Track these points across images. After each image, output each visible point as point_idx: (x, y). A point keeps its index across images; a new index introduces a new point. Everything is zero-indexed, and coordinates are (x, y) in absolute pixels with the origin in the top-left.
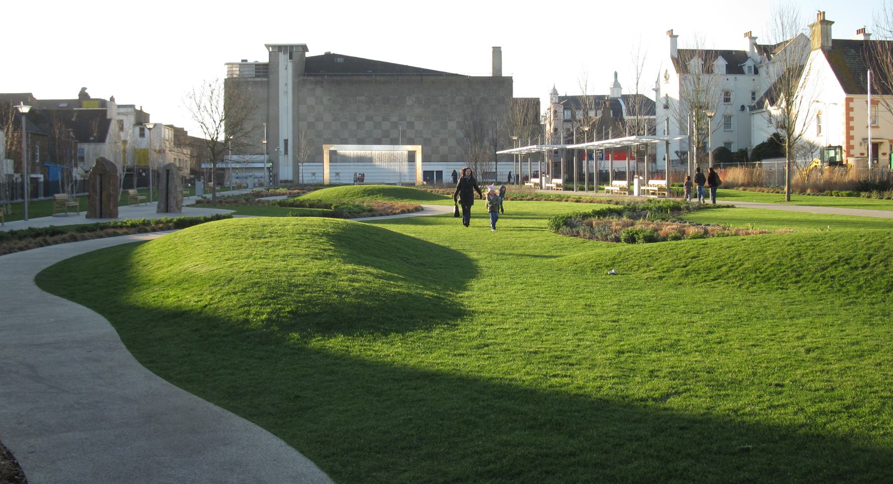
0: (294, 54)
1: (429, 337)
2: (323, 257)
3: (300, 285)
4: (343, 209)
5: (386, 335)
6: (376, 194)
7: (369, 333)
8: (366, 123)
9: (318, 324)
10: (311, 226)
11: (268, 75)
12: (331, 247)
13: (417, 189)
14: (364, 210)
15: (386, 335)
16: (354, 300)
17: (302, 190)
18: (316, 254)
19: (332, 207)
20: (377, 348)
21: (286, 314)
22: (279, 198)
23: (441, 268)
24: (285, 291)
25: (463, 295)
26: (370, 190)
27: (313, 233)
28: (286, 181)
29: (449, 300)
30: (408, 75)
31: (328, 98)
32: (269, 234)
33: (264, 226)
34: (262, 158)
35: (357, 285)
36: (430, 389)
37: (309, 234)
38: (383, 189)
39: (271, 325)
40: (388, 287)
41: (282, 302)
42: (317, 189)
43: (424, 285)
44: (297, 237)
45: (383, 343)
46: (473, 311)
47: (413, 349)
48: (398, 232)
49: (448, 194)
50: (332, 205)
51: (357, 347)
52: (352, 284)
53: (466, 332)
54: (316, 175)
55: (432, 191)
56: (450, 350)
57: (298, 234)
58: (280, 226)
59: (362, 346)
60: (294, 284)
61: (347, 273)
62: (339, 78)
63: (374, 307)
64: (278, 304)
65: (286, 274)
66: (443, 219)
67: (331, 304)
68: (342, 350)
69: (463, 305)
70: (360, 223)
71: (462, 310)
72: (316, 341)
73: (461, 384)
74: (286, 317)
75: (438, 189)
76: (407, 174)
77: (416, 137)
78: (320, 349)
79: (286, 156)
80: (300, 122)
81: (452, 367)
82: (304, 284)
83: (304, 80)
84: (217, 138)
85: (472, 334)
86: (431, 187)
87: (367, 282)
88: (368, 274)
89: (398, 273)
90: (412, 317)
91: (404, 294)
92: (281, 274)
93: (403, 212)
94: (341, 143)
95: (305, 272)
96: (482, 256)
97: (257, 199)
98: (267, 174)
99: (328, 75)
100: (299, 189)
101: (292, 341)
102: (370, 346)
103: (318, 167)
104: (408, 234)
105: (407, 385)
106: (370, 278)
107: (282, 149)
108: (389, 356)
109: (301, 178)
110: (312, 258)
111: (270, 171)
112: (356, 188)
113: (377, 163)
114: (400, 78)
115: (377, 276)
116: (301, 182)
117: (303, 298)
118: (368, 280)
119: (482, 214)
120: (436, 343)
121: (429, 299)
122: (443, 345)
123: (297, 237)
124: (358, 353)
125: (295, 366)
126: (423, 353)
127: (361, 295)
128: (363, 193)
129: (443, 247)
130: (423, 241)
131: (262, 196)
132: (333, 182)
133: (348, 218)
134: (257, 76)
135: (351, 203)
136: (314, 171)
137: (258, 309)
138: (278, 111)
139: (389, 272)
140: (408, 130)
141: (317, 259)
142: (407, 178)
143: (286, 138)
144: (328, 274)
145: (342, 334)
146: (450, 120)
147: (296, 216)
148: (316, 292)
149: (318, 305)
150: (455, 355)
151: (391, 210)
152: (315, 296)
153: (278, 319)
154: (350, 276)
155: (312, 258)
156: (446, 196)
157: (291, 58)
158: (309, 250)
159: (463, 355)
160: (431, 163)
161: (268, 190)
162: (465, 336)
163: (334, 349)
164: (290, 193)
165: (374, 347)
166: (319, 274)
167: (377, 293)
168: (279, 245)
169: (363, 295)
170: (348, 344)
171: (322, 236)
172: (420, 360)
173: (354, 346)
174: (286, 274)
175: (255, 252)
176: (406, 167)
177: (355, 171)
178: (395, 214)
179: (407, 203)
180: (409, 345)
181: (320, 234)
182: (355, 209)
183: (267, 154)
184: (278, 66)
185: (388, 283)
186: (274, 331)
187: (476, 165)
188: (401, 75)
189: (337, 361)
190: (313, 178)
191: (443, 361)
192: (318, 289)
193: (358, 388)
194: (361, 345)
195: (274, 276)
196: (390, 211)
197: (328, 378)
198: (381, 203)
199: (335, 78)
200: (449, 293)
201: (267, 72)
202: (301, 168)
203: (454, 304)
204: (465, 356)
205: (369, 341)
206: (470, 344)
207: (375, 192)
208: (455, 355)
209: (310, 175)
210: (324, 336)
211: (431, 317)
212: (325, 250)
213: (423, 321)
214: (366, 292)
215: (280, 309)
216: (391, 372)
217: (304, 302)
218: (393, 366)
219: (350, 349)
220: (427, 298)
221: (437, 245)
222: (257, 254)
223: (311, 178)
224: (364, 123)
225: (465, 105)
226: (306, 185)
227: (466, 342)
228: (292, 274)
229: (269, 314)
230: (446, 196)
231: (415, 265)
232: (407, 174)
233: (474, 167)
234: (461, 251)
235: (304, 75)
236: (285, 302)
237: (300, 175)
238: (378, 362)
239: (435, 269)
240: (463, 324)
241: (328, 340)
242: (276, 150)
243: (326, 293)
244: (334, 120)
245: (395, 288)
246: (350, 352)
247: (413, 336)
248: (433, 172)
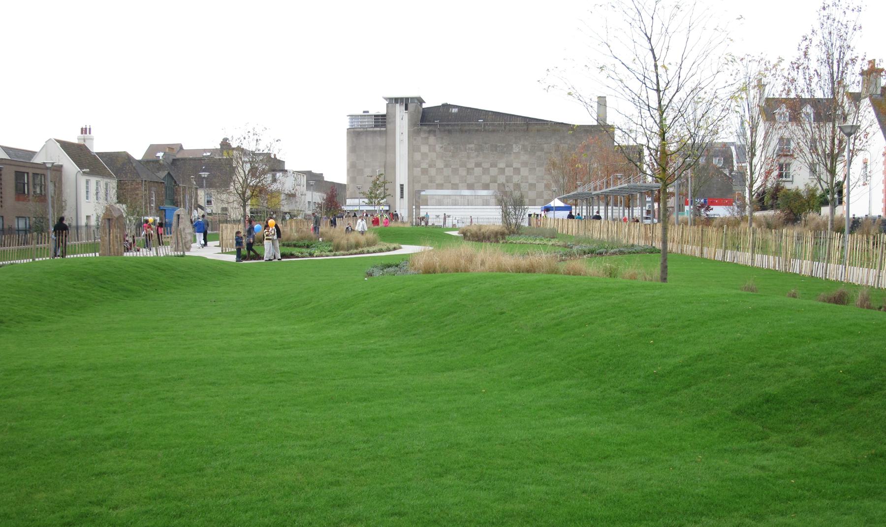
31: (441, 146)
134: (376, 126)
157: (406, 109)
184: (395, 117)
199: (447, 128)
224: (473, 169)
244: (446, 166)
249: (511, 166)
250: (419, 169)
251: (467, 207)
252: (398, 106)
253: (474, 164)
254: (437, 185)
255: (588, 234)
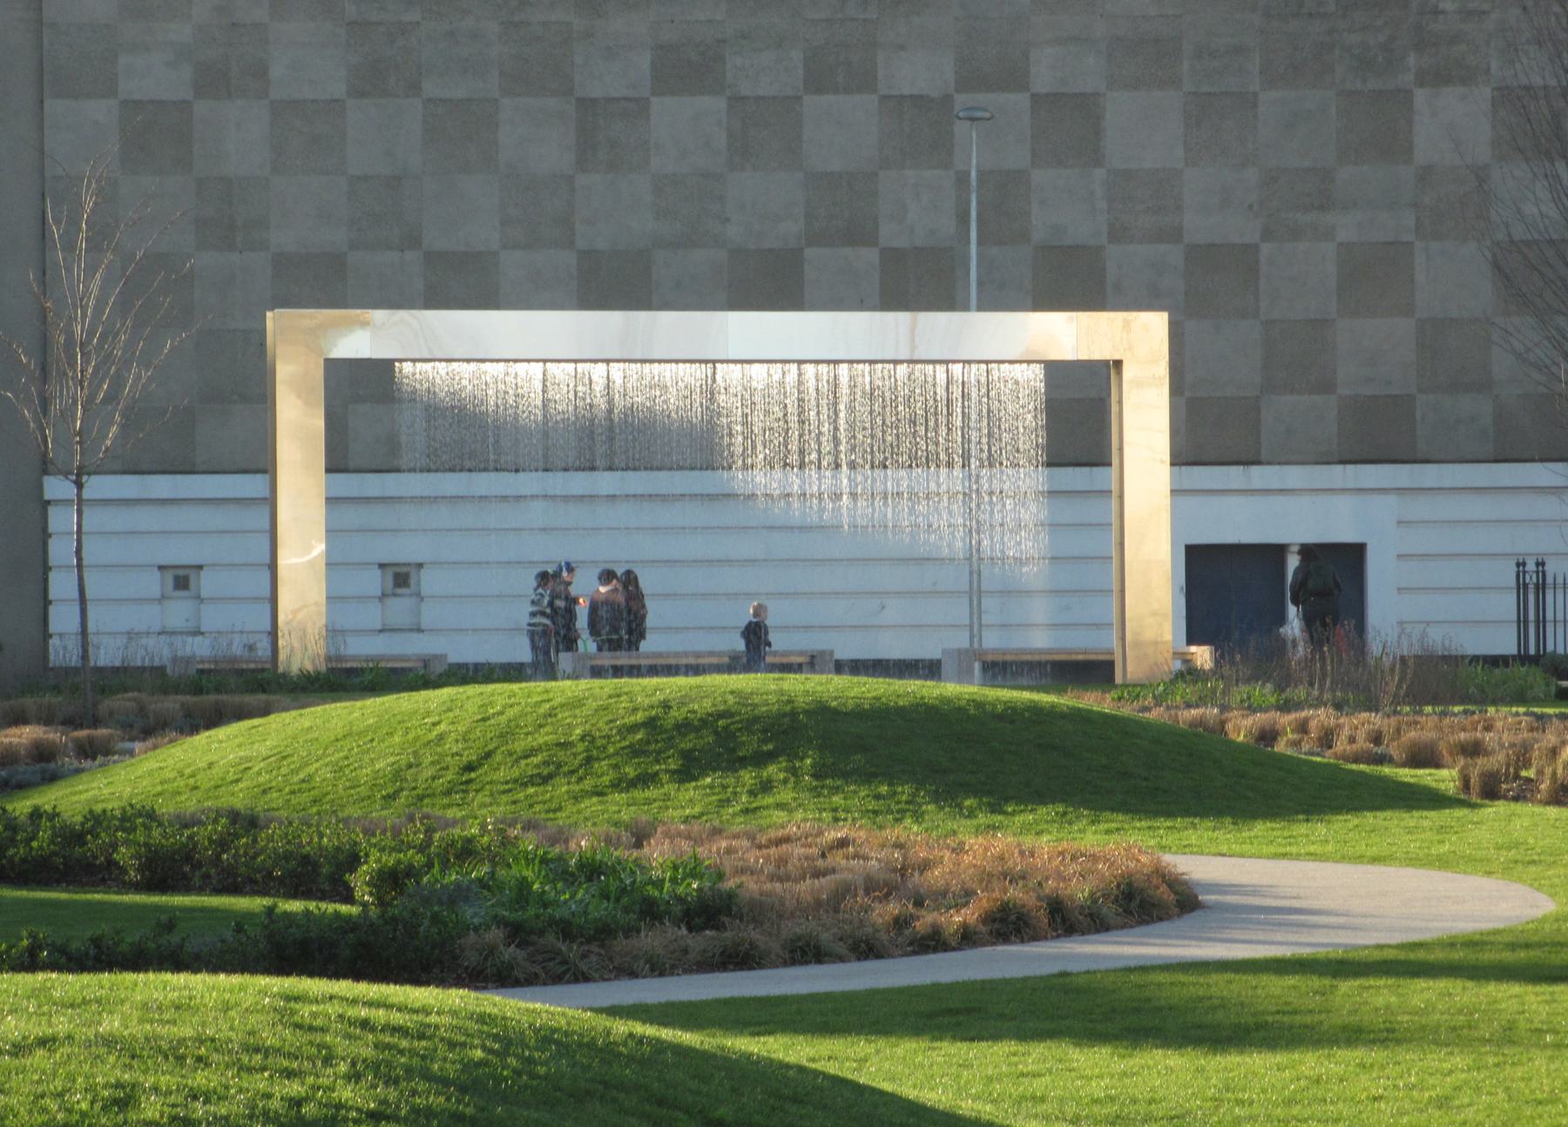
4: (459, 894)
6: (760, 760)
8: (808, 100)
10: (175, 1054)
13: (1126, 711)
14: (651, 912)
17: (71, 722)
19: (360, 881)
38: (823, 710)
42: (215, 718)
49: (1423, 757)
50: (353, 860)
54: (207, 583)
55: (1268, 736)
66: (1381, 995)
70: (621, 1028)
75: (1321, 717)
77: (1118, 234)
80: (54, 107)
84: (964, 368)
86: (1264, 692)
100: (47, 720)
103: (216, 518)
109: (63, 619)
112: (575, 703)
116: (62, 651)
128: (635, 751)
133: (503, 979)
142: (1040, 610)
146: (1438, 77)
151: (893, 908)
156: (1406, 775)
160: (1259, 475)
176: (1033, 512)
177: (551, 552)
178: (933, 943)
179: (1045, 844)
182: (574, 900)
190: (178, 612)
196: (884, 912)
198: (804, 838)
202: (61, 521)
207: (749, 743)
209: (152, 584)
223: (147, 618)
224: (637, 108)
230: (1406, 775)
237: (61, 585)
249: (1013, 77)
250: (100, 111)
251: (579, 483)
253: (644, 62)
255: (253, 654)
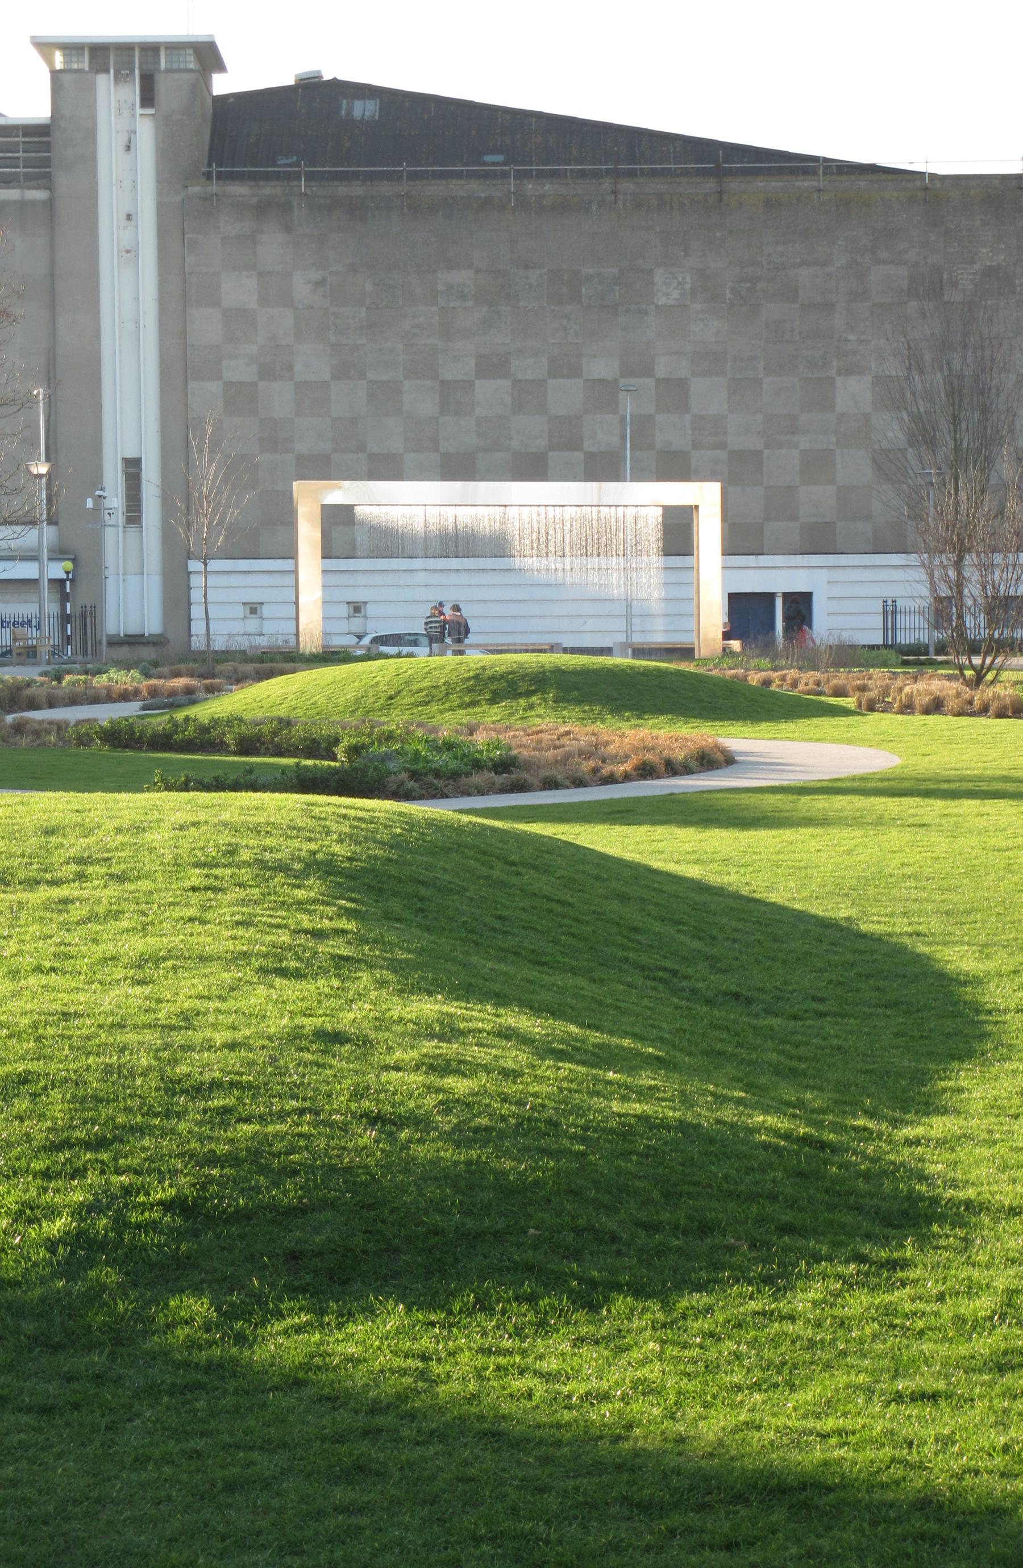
0: (163, 85)
1: (782, 1318)
2: (308, 963)
3: (215, 1085)
4: (387, 757)
5: (593, 1308)
6: (529, 694)
7: (517, 1299)
9: (294, 1256)
10: (256, 830)
11: (48, 176)
12: (343, 924)
13: (701, 671)
14: (477, 765)
15: (593, 1308)
16: (448, 1154)
17: (202, 676)
18: (279, 951)
19: (340, 751)
20: (552, 1364)
21: (155, 1215)
22: (105, 714)
23: (821, 1015)
24: (151, 1113)
25: (920, 1131)
26: (503, 676)
27: (262, 864)
28: (134, 641)
29: (865, 1156)
30: (662, 173)
31: (316, 275)
32: (73, 868)
33: (50, 832)
34: (29, 537)
35: (460, 1085)
36: (794, 1550)
37: (247, 864)
39: (92, 1264)
40: (598, 1094)
41: (134, 1161)
42: (270, 674)
43: (749, 1087)
44: (195, 877)
45: (580, 1341)
46: (968, 1204)
47: (712, 1368)
48: (628, 856)
50: (337, 741)
51: (464, 1357)
52: (438, 1082)
53: (941, 1298)
54: (266, 611)
55: (767, 683)
56: (875, 1374)
57: (197, 865)
58: (119, 830)
59: (486, 1352)
60: (187, 1084)
61: (416, 1035)
62: (357, 189)
63: (536, 1183)
64: (119, 1172)
65: (152, 1037)
66: (821, 803)
67: (348, 1170)
68: (404, 1372)
69: (922, 1178)
70: (466, 819)
71: (921, 1198)
72: (285, 1332)
73: (932, 1527)
74: (153, 1226)
75: (792, 673)
76: (657, 608)
78: (306, 1367)
79: (133, 530)
80: (192, 384)
81: (888, 1452)
82: (232, 1084)
83: (207, 199)
85: (967, 1307)
86: (766, 662)
87: (507, 1074)
88: (508, 1038)
89: (635, 1036)
90: (705, 1229)
91: (664, 1125)
92: (130, 1037)
93: (646, 771)
94: (374, 475)
95: (234, 1028)
96: (999, 961)
97: (9, 718)
98: (51, 607)
99: (311, 177)
100: (191, 675)
101: (181, 1333)
102: (524, 1353)
104: (671, 867)
105: (690, 1530)
106: (515, 1057)
107: (115, 500)
108: (605, 1397)
109: (198, 628)
110: (263, 971)
111: (64, 598)
113: (531, 562)
114: (627, 186)
115: (546, 1050)
116: (198, 643)
117: (231, 1141)
118: (510, 1064)
119: (993, 779)
120: (812, 1344)
121: (777, 1150)
122: (844, 1354)
123: (195, 881)
124: (472, 1386)
125: (199, 1443)
126: (756, 1387)
127: (477, 1130)
128: (470, 690)
129: (826, 924)
130: (737, 896)
131: (33, 705)
132: (340, 641)
133: (407, 796)
135: (419, 733)
136: (254, 597)
137: (33, 1192)
138: (97, 334)
139: (597, 1028)
140: (660, 418)
141: (283, 973)
142: (659, 624)
143: (131, 454)
144: (337, 1038)
145: (401, 1299)
146: (847, 371)
147: (185, 788)
148: (282, 1116)
149: (295, 1173)
150: (899, 1398)
151: (592, 763)
152: (280, 1136)
153: (120, 1234)
154: (428, 1046)
155: (263, 971)
156: (832, 700)
157: (148, 99)
158: (249, 934)
159: (933, 1397)
161: (59, 678)
162: (937, 1314)
163: (363, 1368)
164: (154, 692)
165: (540, 1357)
166: (294, 1037)
167: (549, 1122)
168: (117, 915)
169: (487, 1129)
170: (426, 1343)
171: (304, 873)
172: (742, 1418)
173: (452, 1354)
174: (152, 1037)
175: (13, 946)
177: (438, 596)
178: (610, 780)
180: (696, 1352)
181: (297, 866)
183: (51, 521)
184: (91, 135)
185: (596, 1079)
186: (104, 1288)
187: (958, 565)
188: (632, 174)
189: (380, 1421)
190: (252, 625)
191: (848, 1423)
192: (295, 1104)
193: (477, 1540)
194: (481, 1350)
195: (101, 1050)
196: (587, 765)
197: (340, 1494)
199: (342, 189)
200: (860, 1122)
201: (47, 163)
202: (196, 581)
203: (884, 1173)
204: (942, 1403)
205: (518, 1333)
206: (963, 1350)
207: (523, 686)
208: (899, 1398)
209: (240, 611)
210: (323, 1312)
211: (786, 1229)
212: (318, 935)
213: (752, 1246)
214: (503, 1118)
215: (127, 1191)
216: (619, 1467)
217: (232, 1160)
218: (627, 1445)
219: (437, 1369)
220: (766, 1146)
221: (801, 916)
222: (20, 952)
223: (237, 627)
224: (468, 386)
225: (913, 305)
226: (225, 656)
227: (945, 1338)
228: (178, 1038)
229: (83, 1211)
230: (832, 700)
231: (708, 1002)
232: (657, 608)
233: (952, 574)
234: (907, 941)
235: (208, 176)
236: (150, 1159)
238: (558, 1426)
239: (796, 1018)
240: (933, 1257)
241: (340, 1326)
242: (89, 503)
243: (326, 1123)
244: (343, 372)
245: (624, 1099)
246: (435, 1382)
247: (709, 1310)
248: (770, 597)
249: (647, 371)
250: (214, 387)
252: (104, 83)
253: (472, 363)
254: (590, 457)
